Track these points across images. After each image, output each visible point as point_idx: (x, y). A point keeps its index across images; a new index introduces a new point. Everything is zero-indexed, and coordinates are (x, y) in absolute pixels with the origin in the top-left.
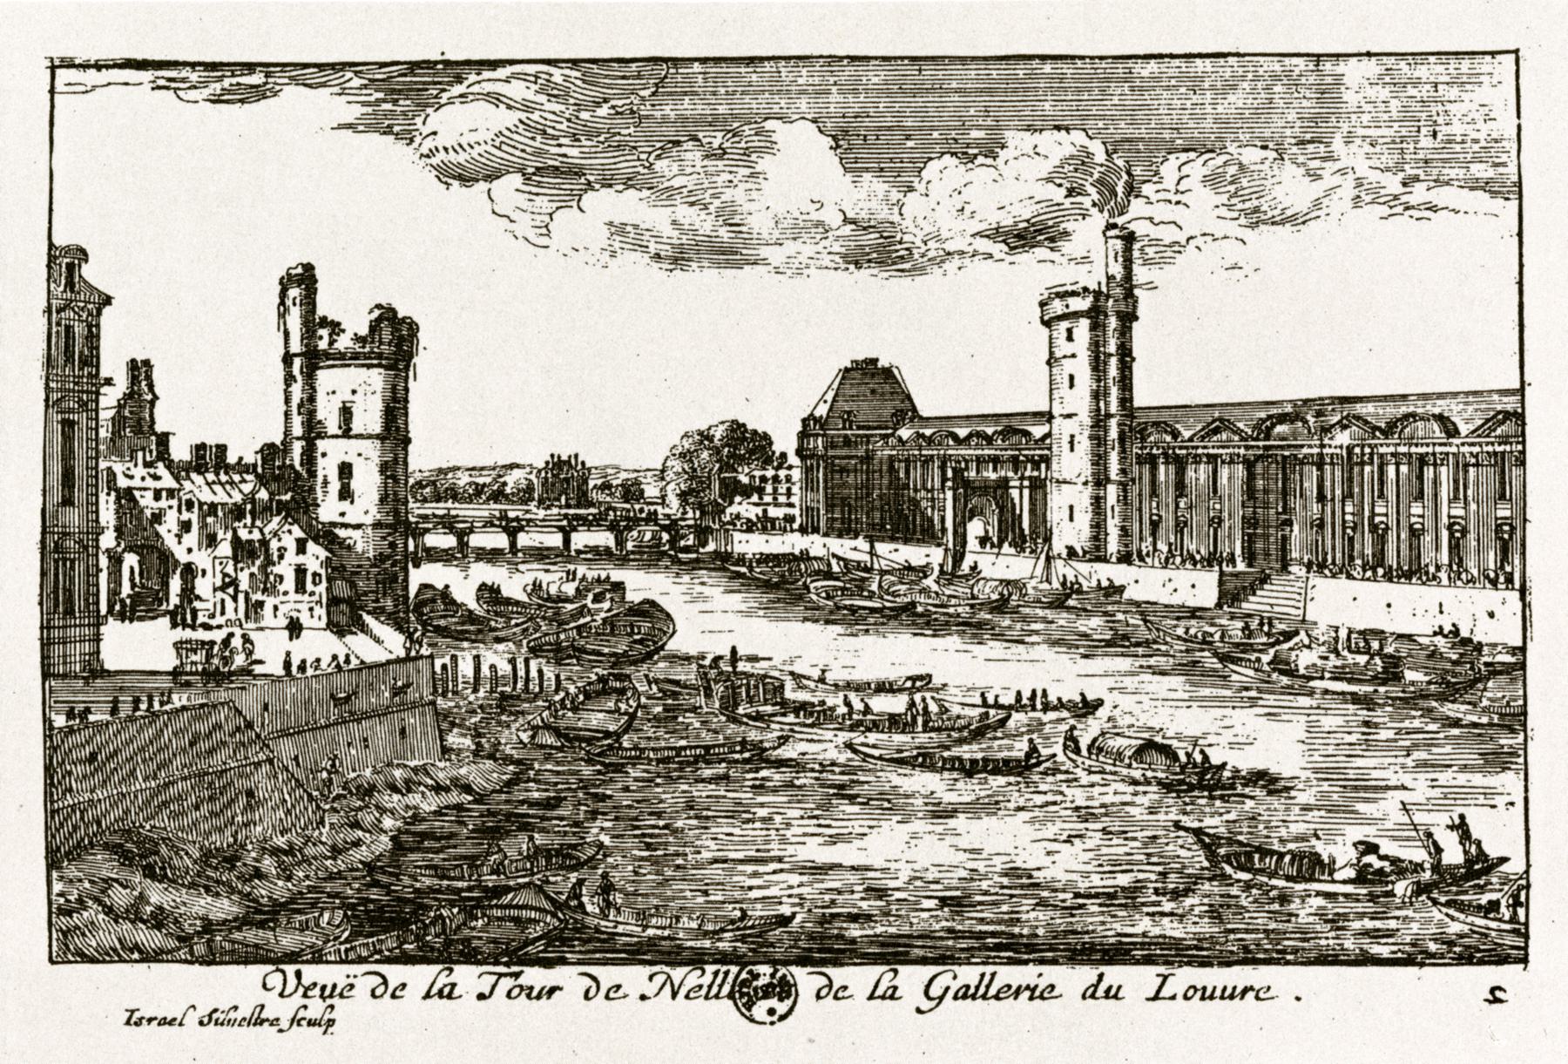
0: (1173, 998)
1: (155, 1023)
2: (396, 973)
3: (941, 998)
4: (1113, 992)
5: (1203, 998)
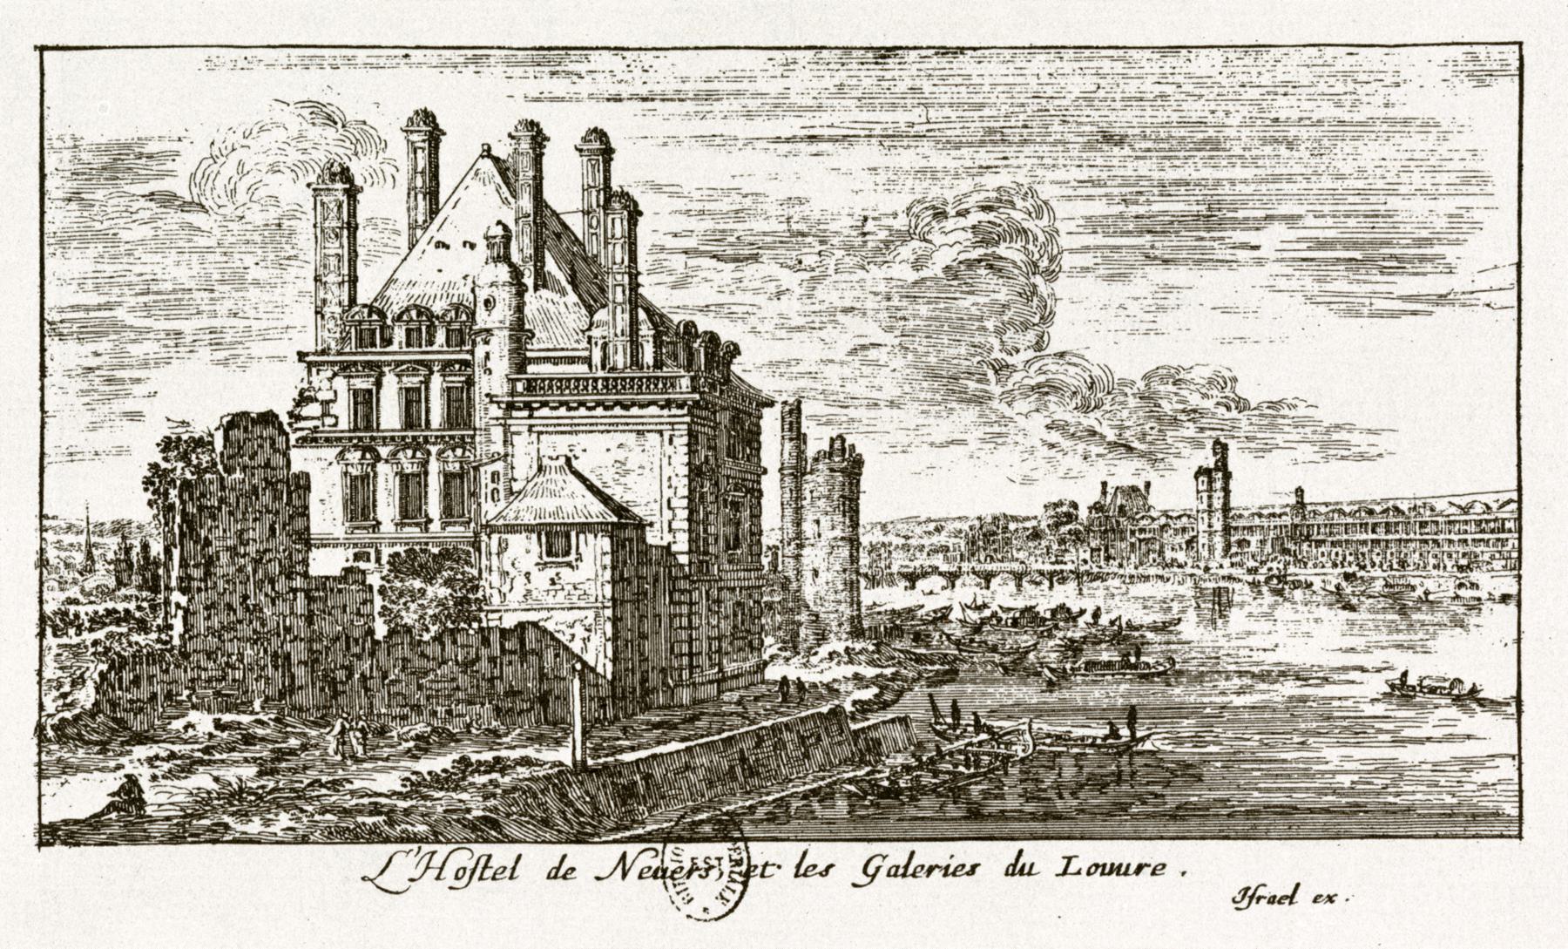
0: (1079, 873)
1: (937, 873)
2: (820, 853)
3: (874, 876)
4: (1026, 870)
5: (1102, 874)
